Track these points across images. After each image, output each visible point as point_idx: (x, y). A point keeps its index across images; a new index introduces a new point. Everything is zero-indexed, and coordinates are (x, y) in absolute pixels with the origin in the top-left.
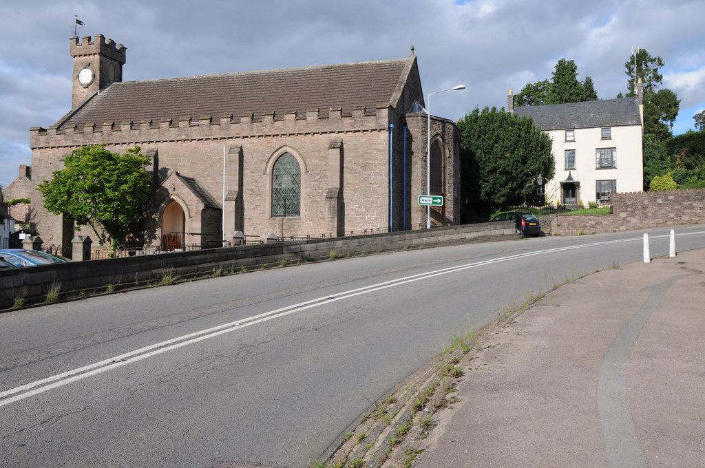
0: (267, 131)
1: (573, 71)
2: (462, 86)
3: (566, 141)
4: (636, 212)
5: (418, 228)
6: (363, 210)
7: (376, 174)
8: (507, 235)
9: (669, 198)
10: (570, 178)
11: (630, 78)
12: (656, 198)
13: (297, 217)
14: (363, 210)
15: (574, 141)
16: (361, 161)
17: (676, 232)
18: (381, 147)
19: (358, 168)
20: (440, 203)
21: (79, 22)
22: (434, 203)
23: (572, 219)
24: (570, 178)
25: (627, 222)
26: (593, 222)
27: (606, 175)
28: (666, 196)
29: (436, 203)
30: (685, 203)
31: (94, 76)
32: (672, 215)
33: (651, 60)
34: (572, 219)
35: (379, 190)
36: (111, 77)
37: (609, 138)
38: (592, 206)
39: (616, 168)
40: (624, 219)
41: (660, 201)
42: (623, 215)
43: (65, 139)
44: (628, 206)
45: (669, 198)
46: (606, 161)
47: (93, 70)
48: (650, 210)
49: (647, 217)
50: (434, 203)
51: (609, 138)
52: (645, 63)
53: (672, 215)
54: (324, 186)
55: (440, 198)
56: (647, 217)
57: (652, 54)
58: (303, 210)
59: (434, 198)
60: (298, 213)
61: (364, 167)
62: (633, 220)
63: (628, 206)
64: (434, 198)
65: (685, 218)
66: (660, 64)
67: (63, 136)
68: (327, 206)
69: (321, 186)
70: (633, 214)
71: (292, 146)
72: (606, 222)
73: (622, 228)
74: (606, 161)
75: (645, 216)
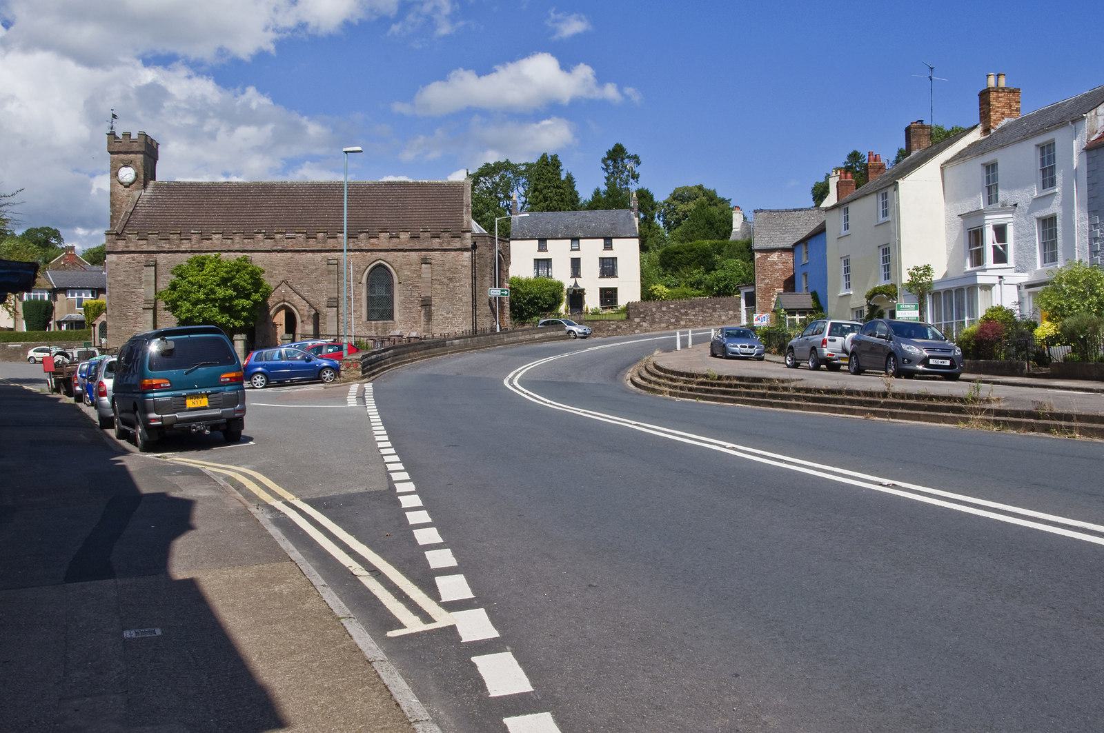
0: (363, 245)
1: (558, 167)
2: (359, 148)
3: (572, 250)
4: (647, 318)
5: (237, 337)
6: (451, 316)
7: (462, 286)
8: (561, 336)
9: (671, 306)
10: (576, 284)
11: (606, 175)
12: (661, 306)
13: (391, 321)
14: (451, 316)
15: (579, 250)
16: (448, 274)
17: (681, 333)
18: (465, 263)
19: (445, 280)
20: (507, 295)
21: (114, 116)
22: (501, 294)
23: (598, 324)
24: (576, 284)
25: (640, 326)
26: (615, 326)
27: (608, 283)
28: (669, 305)
29: (504, 294)
30: (683, 311)
31: (137, 175)
32: (673, 320)
33: (628, 157)
34: (598, 324)
35: (465, 299)
36: (149, 176)
37: (611, 248)
38: (595, 313)
39: (617, 277)
40: (638, 323)
41: (664, 309)
42: (637, 320)
43: (148, 244)
44: (641, 313)
45: (671, 306)
46: (608, 267)
47: (136, 168)
48: (657, 316)
49: (655, 322)
50: (501, 294)
51: (611, 248)
52: (622, 160)
53: (673, 320)
54: (416, 295)
55: (507, 291)
56: (655, 322)
57: (630, 151)
58: (397, 316)
59: (502, 291)
60: (391, 317)
61: (450, 279)
62: (645, 324)
63: (641, 313)
64: (502, 291)
65: (683, 323)
66: (638, 163)
67: (145, 242)
68: (423, 312)
69: (413, 294)
70: (644, 320)
71: (391, 260)
72: (624, 327)
73: (637, 331)
74: (608, 267)
75: (653, 322)
